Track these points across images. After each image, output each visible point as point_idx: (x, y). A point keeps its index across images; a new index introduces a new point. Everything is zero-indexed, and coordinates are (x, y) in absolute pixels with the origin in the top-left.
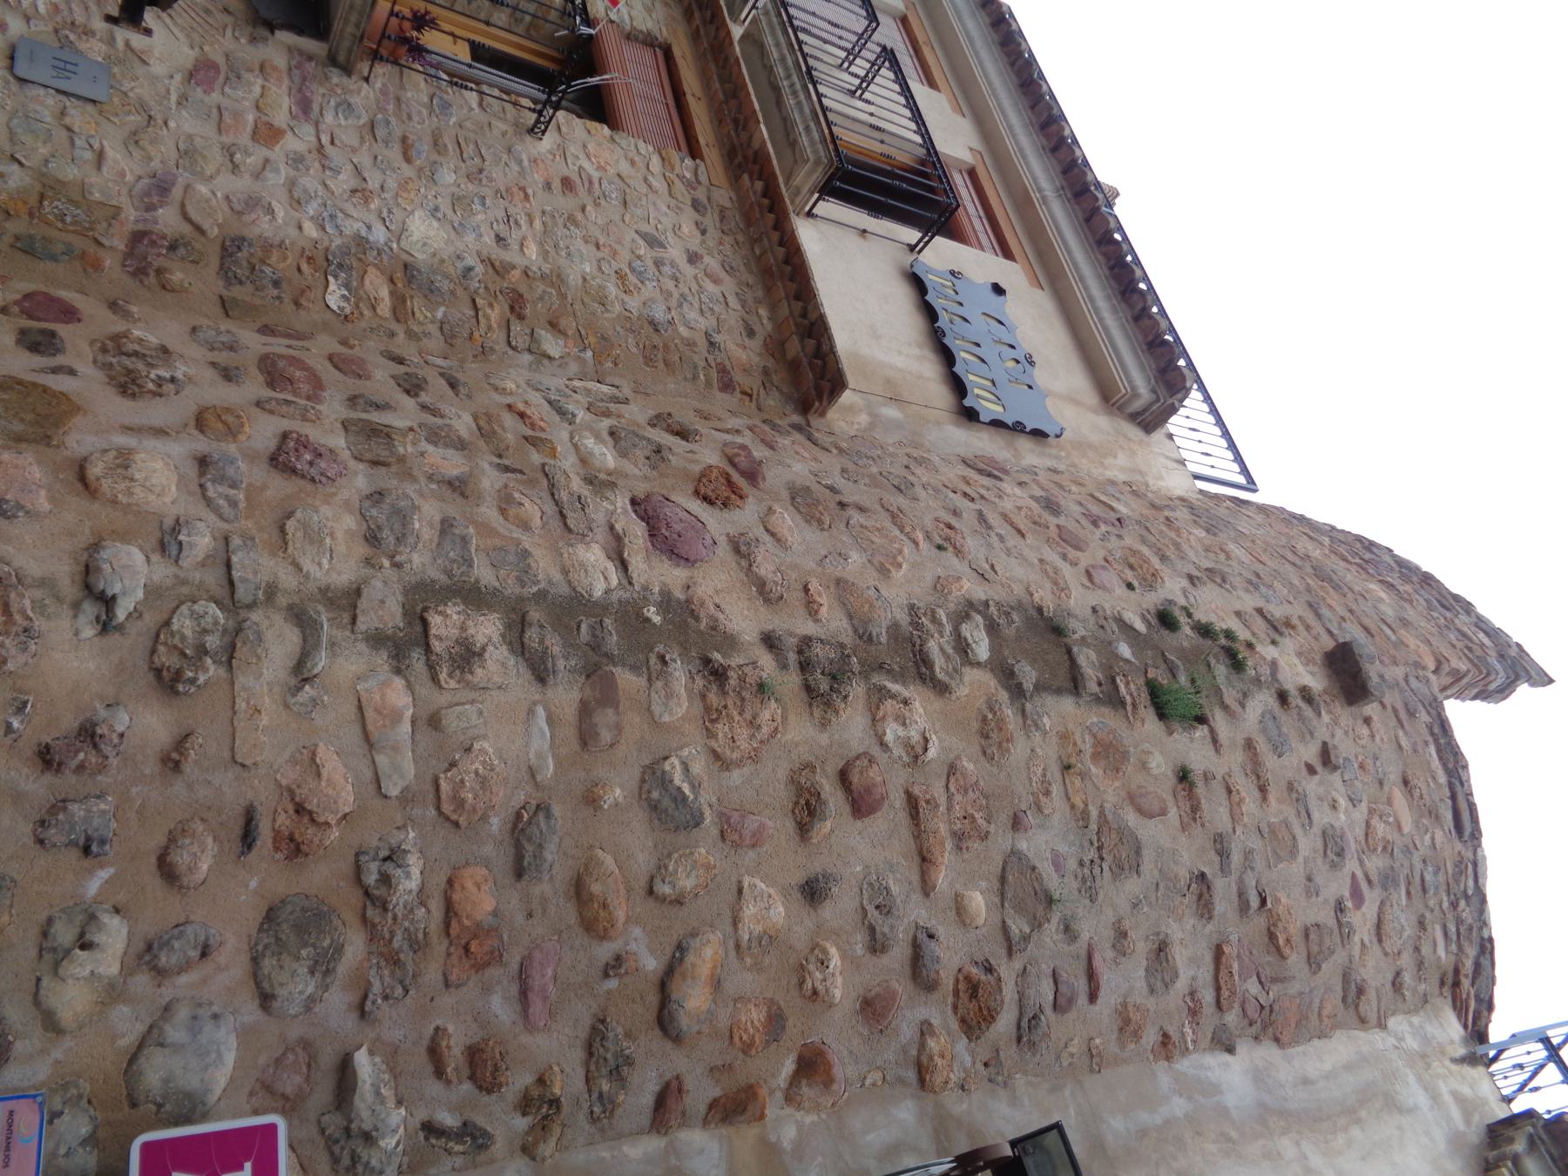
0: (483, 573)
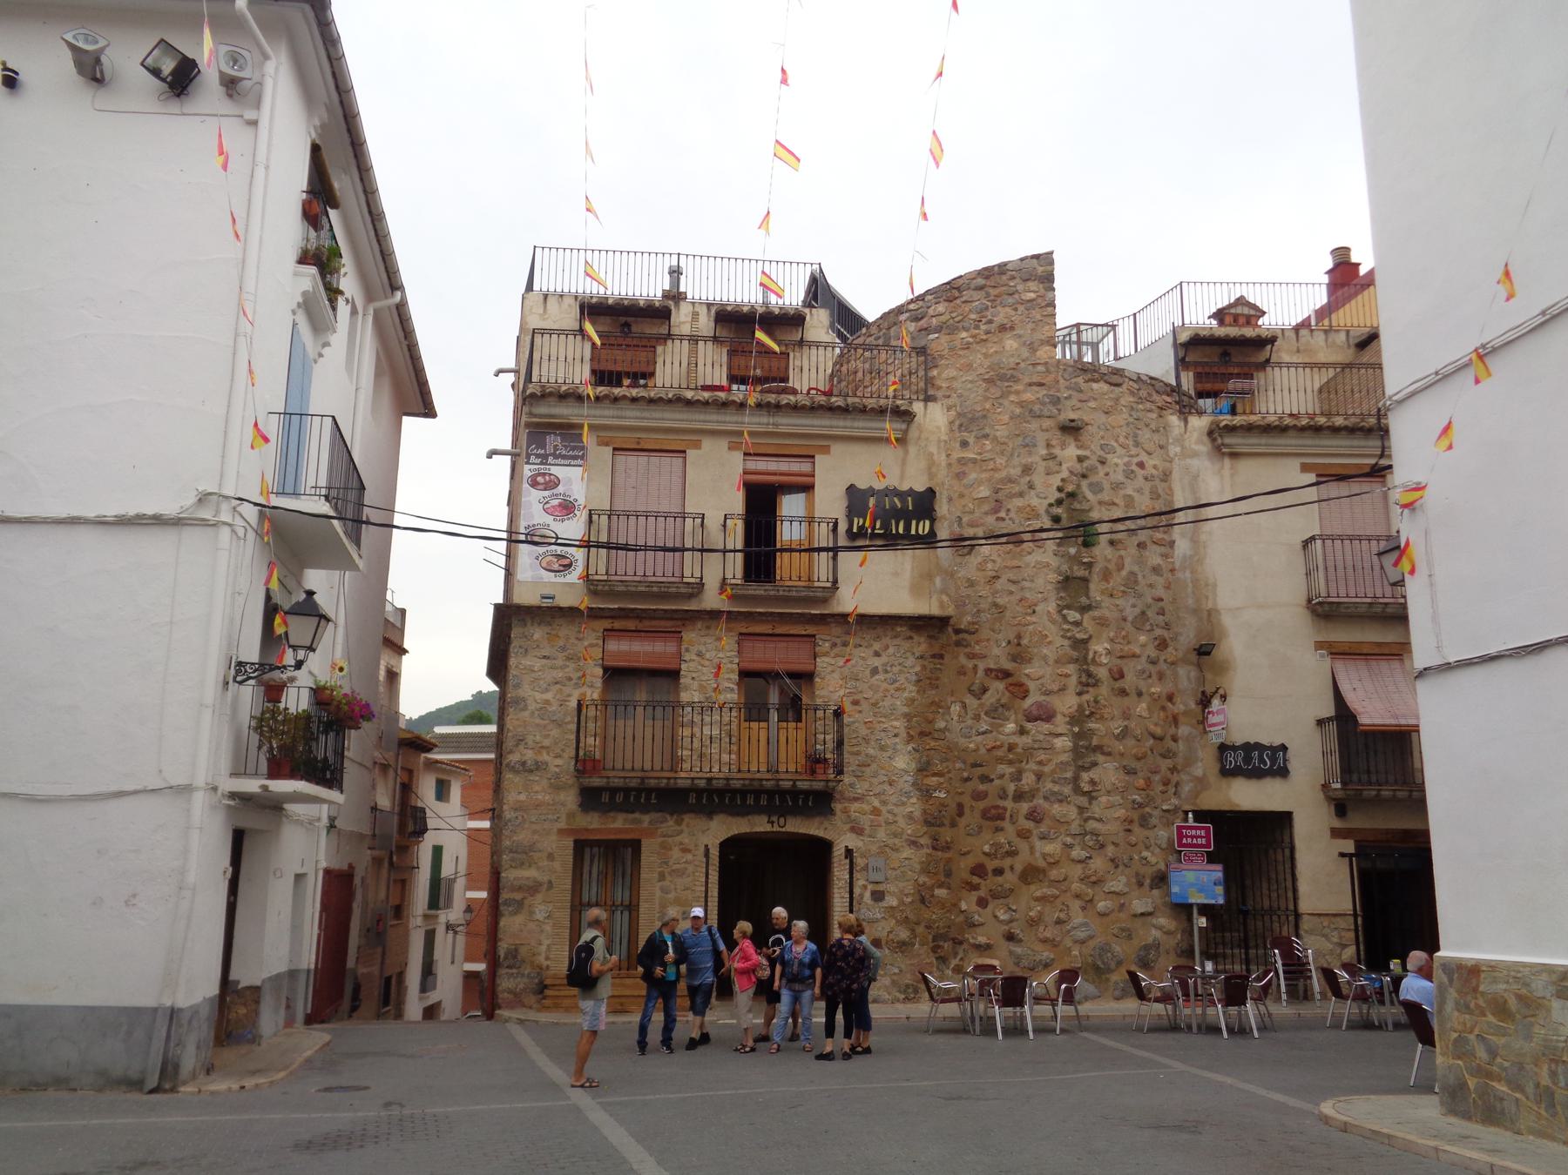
0: (1069, 775)
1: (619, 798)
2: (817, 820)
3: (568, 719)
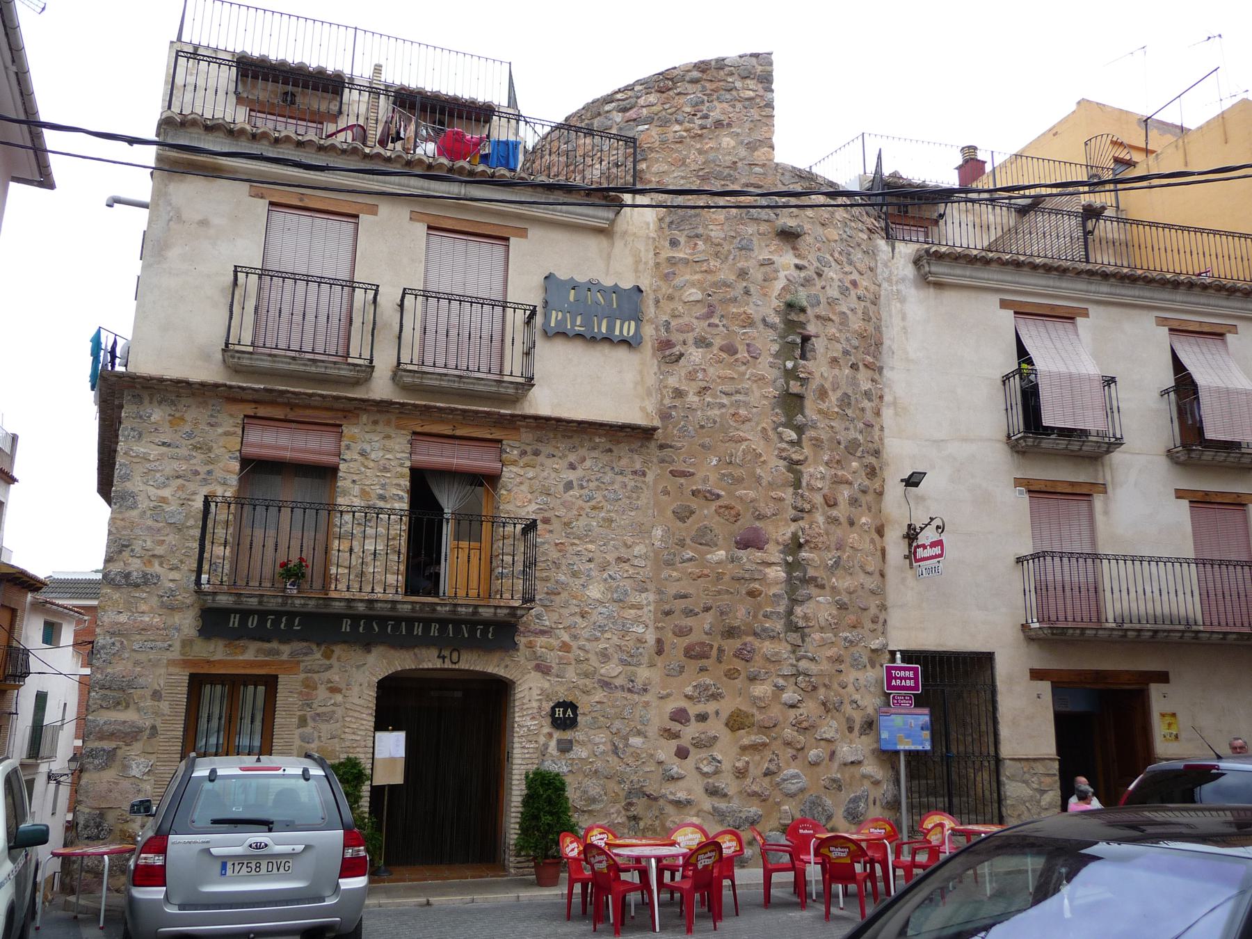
1: (252, 622)
2: (496, 657)
3: (191, 522)
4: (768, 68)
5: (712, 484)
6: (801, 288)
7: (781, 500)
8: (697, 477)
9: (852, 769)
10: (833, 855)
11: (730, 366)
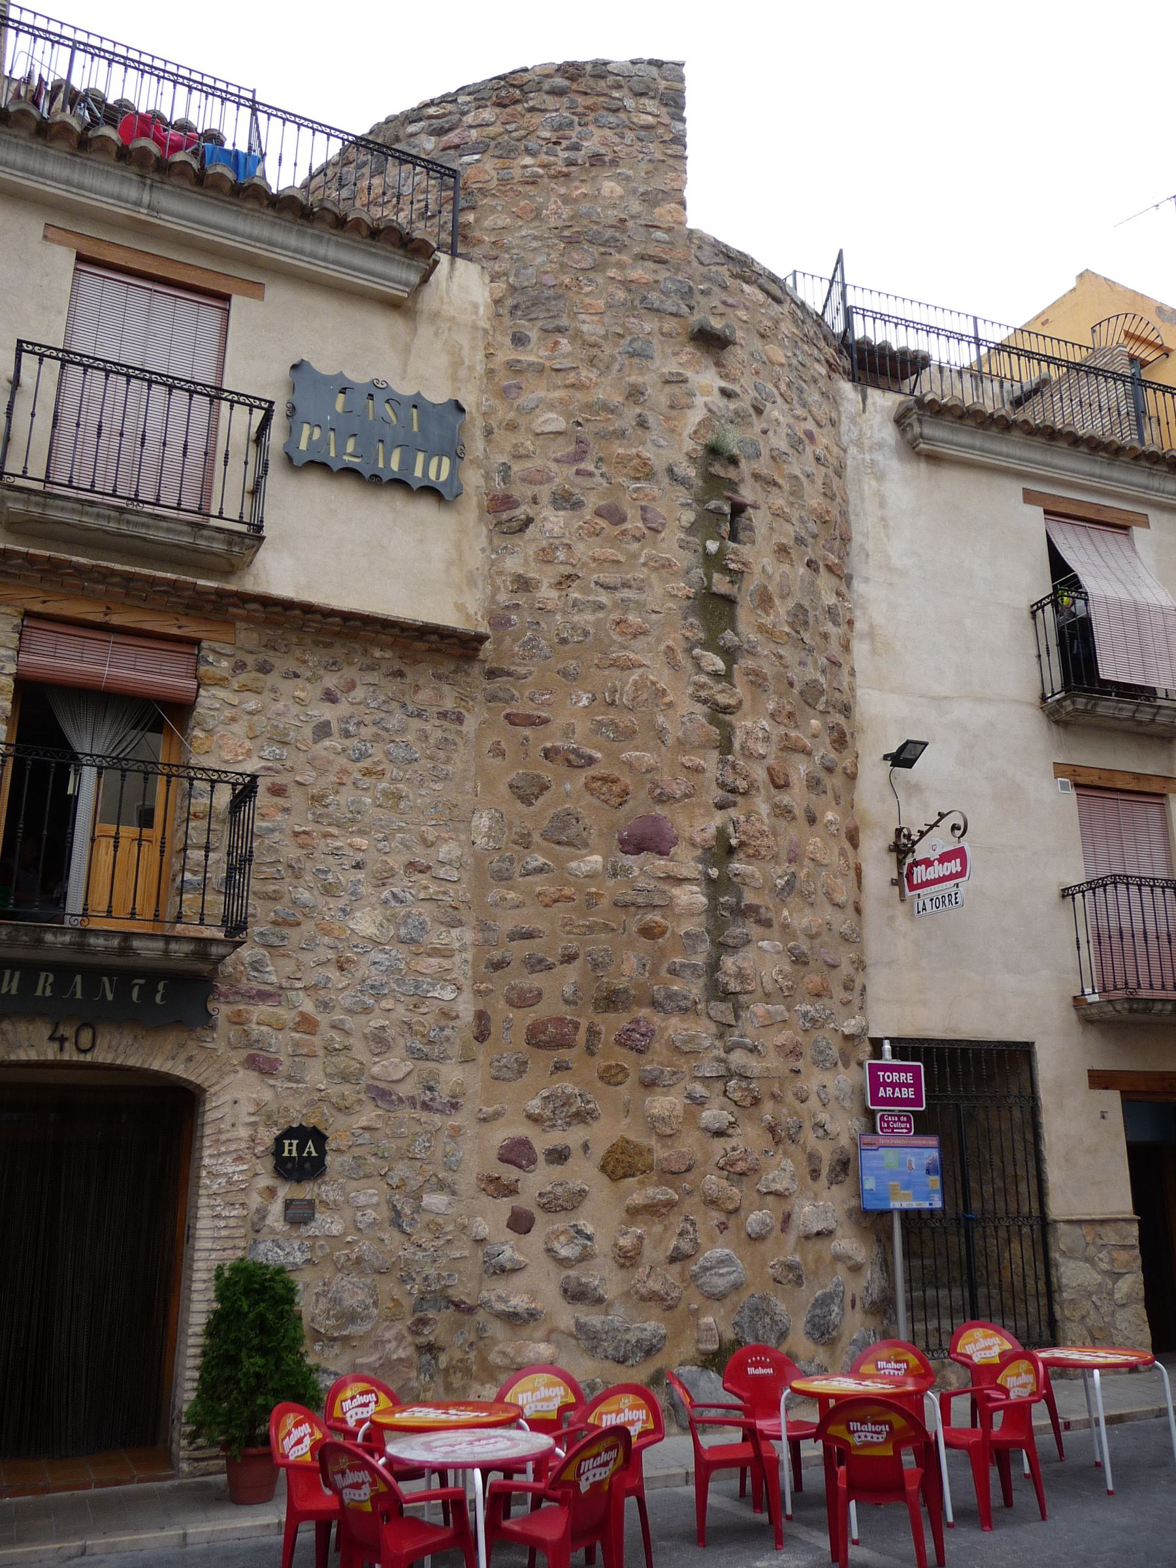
0: (700, 960)
2: (170, 1041)
4: (677, 85)
5: (581, 739)
6: (729, 426)
7: (699, 770)
8: (552, 727)
9: (819, 1245)
10: (855, 1440)
11: (614, 541)
